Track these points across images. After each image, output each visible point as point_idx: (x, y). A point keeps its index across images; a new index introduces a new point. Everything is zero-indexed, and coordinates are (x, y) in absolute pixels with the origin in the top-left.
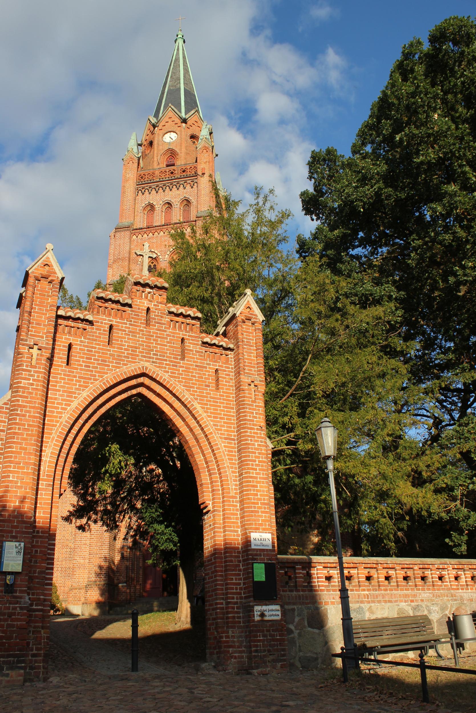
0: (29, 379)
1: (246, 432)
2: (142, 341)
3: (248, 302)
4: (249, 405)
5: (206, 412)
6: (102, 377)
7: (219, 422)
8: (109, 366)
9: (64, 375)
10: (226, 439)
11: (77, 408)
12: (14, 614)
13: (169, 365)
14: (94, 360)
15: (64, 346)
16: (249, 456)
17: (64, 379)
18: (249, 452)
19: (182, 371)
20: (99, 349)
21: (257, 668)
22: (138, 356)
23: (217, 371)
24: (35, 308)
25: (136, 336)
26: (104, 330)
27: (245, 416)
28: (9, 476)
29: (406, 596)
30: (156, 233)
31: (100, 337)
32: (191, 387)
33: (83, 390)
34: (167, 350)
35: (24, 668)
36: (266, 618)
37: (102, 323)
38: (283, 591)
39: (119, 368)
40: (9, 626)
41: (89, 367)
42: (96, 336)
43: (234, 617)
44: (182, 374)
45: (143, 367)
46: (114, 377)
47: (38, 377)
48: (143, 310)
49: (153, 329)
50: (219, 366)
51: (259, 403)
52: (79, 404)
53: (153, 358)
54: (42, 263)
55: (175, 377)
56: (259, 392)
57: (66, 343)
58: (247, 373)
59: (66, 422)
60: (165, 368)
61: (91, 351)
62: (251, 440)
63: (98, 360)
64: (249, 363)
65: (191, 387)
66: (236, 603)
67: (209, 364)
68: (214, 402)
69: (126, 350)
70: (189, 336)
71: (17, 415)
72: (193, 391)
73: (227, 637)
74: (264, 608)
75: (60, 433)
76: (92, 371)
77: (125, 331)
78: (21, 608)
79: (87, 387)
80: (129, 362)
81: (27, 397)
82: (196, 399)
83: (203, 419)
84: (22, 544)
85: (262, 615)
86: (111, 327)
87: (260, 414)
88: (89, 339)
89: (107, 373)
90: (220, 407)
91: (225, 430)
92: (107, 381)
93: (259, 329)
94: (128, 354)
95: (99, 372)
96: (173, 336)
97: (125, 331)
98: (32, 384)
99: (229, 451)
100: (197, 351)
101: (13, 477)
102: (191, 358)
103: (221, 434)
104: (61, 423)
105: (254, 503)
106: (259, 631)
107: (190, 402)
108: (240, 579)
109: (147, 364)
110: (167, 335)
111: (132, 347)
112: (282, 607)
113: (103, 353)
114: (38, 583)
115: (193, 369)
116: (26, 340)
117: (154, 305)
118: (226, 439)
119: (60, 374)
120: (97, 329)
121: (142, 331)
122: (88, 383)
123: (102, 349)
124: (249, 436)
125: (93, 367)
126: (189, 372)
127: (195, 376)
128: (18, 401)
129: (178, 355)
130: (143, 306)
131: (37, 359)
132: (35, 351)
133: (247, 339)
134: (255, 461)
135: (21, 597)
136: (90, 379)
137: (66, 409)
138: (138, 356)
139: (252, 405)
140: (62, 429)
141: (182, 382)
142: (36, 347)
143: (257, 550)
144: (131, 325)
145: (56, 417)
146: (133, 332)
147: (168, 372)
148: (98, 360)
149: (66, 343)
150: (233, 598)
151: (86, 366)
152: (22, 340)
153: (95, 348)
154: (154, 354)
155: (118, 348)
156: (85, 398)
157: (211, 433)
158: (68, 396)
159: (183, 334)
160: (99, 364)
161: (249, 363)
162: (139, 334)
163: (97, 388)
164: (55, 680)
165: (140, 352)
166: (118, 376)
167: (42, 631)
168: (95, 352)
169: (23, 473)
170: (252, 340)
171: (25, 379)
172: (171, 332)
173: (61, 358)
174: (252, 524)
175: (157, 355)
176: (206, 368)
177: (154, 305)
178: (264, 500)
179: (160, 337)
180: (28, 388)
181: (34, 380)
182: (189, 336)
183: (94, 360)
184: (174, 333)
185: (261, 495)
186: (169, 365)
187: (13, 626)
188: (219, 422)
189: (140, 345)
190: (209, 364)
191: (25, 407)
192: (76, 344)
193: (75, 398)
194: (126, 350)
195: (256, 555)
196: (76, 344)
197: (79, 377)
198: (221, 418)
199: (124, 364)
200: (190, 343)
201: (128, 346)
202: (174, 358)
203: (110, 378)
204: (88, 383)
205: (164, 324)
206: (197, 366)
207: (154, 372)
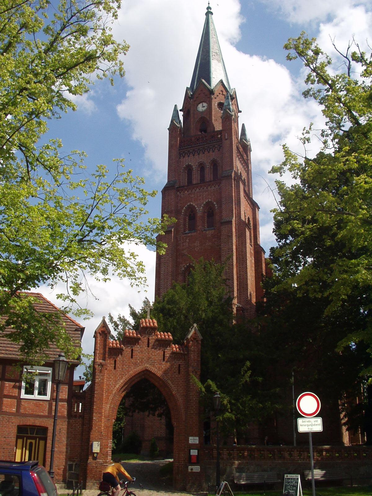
23: (179, 365)
74: (193, 467)
85: (192, 469)
171: (98, 379)
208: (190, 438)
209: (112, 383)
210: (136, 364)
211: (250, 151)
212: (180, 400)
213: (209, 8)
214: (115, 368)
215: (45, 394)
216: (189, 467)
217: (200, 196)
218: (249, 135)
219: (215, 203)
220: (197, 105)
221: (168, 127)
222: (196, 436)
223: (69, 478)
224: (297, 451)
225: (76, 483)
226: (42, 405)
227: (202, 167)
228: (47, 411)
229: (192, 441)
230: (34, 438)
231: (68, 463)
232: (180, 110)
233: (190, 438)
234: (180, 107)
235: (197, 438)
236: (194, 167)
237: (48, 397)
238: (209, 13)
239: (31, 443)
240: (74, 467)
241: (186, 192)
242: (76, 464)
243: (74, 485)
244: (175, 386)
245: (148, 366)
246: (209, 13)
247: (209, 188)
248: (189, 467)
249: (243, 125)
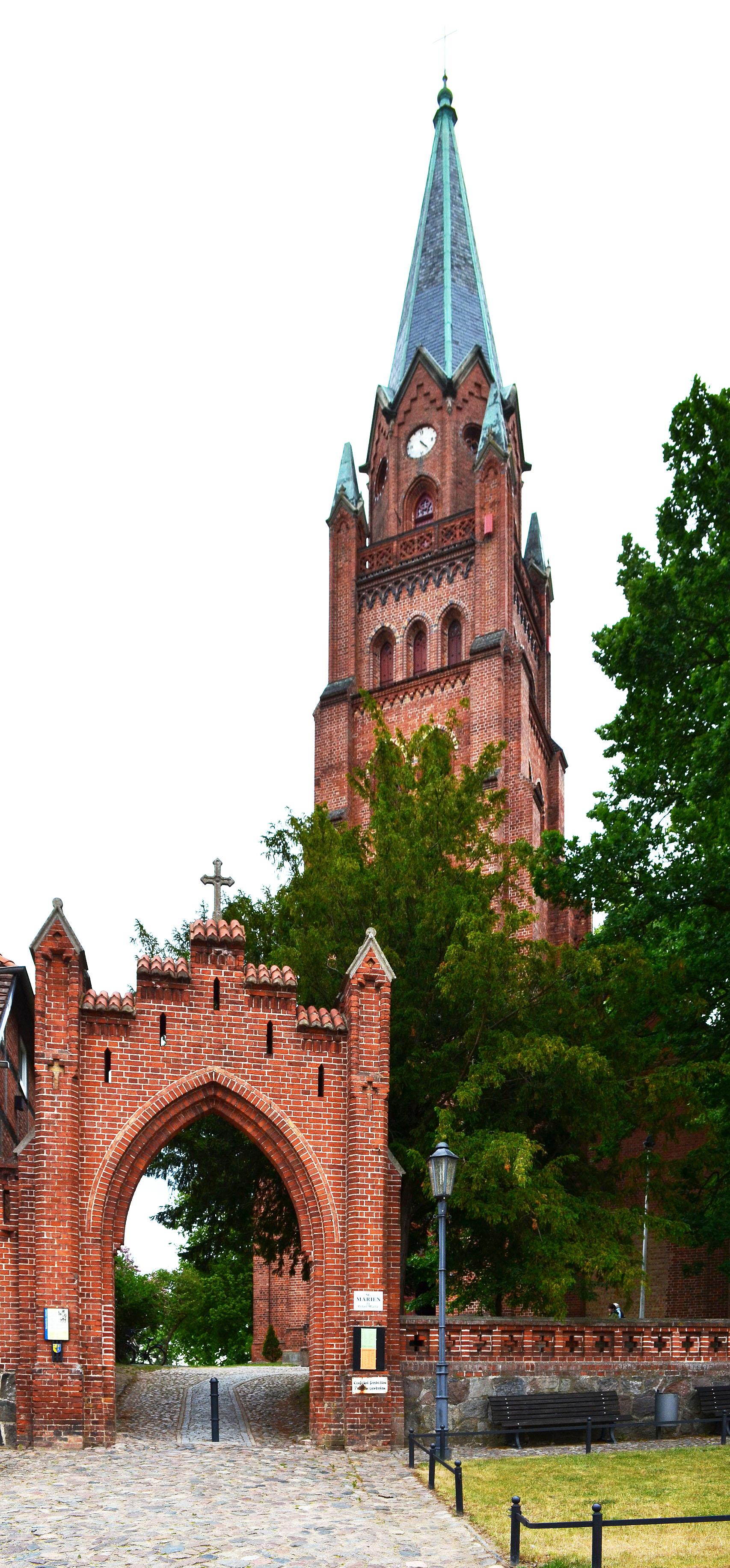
0: (53, 1110)
1: (356, 1158)
3: (371, 950)
4: (362, 1118)
5: (303, 1131)
6: (154, 1094)
7: (321, 1144)
9: (103, 1096)
11: (123, 1140)
12: (66, 1383)
13: (249, 1066)
14: (142, 1070)
15: (99, 1055)
16: (357, 1191)
17: (103, 1102)
18: (358, 1186)
19: (269, 1073)
20: (147, 1053)
21: (352, 1444)
22: (203, 1057)
24: (50, 1005)
25: (199, 1028)
26: (153, 1024)
27: (355, 1135)
28: (43, 1235)
29: (592, 1367)
32: (282, 1097)
33: (130, 1115)
34: (246, 1043)
36: (365, 1392)
37: (149, 1013)
38: (409, 1359)
39: (177, 1078)
40: (61, 1394)
41: (135, 1081)
42: (143, 1035)
43: (333, 1389)
44: (268, 1079)
45: (211, 1074)
47: (64, 1105)
50: (325, 1060)
51: (377, 1114)
52: (126, 1135)
53: (225, 1059)
57: (101, 1049)
58: (363, 1069)
59: (111, 1159)
60: (244, 1071)
61: (137, 1058)
62: (362, 1169)
63: (147, 1070)
64: (367, 1052)
65: (282, 1097)
66: (337, 1373)
67: (310, 1059)
68: (315, 1115)
69: (185, 1050)
70: (280, 1017)
72: (285, 1102)
73: (322, 1410)
75: (105, 1174)
76: (140, 1087)
77: (183, 1021)
78: (73, 1377)
79: (134, 1110)
80: (191, 1067)
81: (52, 1134)
82: (289, 1114)
84: (66, 1311)
85: (362, 1388)
88: (132, 1040)
89: (161, 1088)
91: (330, 1156)
93: (386, 996)
94: (189, 1056)
95: (149, 1088)
96: (255, 1021)
97: (183, 1021)
98: (57, 1116)
99: (335, 1184)
100: (291, 1041)
101: (48, 1235)
102: (282, 1052)
103: (324, 1161)
104: (105, 1161)
107: (279, 1118)
108: (343, 1346)
109: (217, 1069)
110: (246, 1020)
111: (194, 1045)
112: (389, 1379)
113: (153, 1059)
114: (93, 1350)
115: (286, 1069)
117: (226, 974)
119: (97, 1096)
120: (142, 1024)
121: (209, 1018)
122: (135, 1104)
123: (152, 1053)
124: (359, 1163)
125: (141, 1081)
126: (278, 1074)
127: (288, 1080)
128: (43, 1140)
129: (263, 1050)
130: (208, 978)
131: (60, 1081)
132: (56, 1070)
133: (366, 1013)
134: (366, 1197)
135: (71, 1366)
136: (138, 1098)
138: (203, 1057)
140: (107, 1170)
141: (268, 1090)
144: (191, 1010)
145: (98, 1154)
147: (247, 1077)
149: (101, 1049)
150: (333, 1367)
151: (131, 1081)
153: (142, 1052)
154: (226, 1053)
155: (174, 1049)
156: (133, 1126)
157: (310, 1160)
158: (110, 1125)
159: (269, 1016)
160: (148, 1076)
161: (367, 1052)
162: (204, 1023)
164: (119, 1446)
165: (206, 1052)
166: (176, 1090)
167: (103, 1399)
168: (143, 1058)
169: (60, 1230)
170: (375, 1014)
171: (48, 1110)
172: (252, 1015)
173: (96, 1073)
174: (356, 1280)
176: (304, 1065)
177: (226, 974)
178: (376, 1248)
179: (234, 1025)
180: (53, 1122)
182: (280, 1017)
183: (142, 1070)
184: (256, 1016)
185: (372, 1243)
186: (249, 1066)
187: (66, 1395)
188: (321, 1144)
189: (205, 1040)
190: (310, 1059)
191: (51, 1146)
192: (115, 1050)
194: (185, 1050)
195: (360, 1318)
196: (115, 1050)
197: (123, 1097)
198: (324, 1138)
199: (184, 1073)
200: (280, 1029)
201: (188, 1044)
202: (256, 1055)
203: (165, 1093)
205: (241, 1003)
206: (290, 1064)
207: (227, 1080)
208: (357, 1294)
209: (102, 1125)
210: (176, 1066)
211: (550, 598)
212: (324, 1178)
213: (445, 94)
216: (354, 1380)
217: (414, 716)
218: (549, 553)
220: (408, 440)
221: (328, 516)
222: (374, 1288)
227: (418, 629)
232: (363, 469)
233: (357, 1294)
234: (361, 459)
236: (397, 634)
238: (446, 113)
246: (446, 113)
247: (438, 691)
248: (354, 1380)
249: (534, 518)
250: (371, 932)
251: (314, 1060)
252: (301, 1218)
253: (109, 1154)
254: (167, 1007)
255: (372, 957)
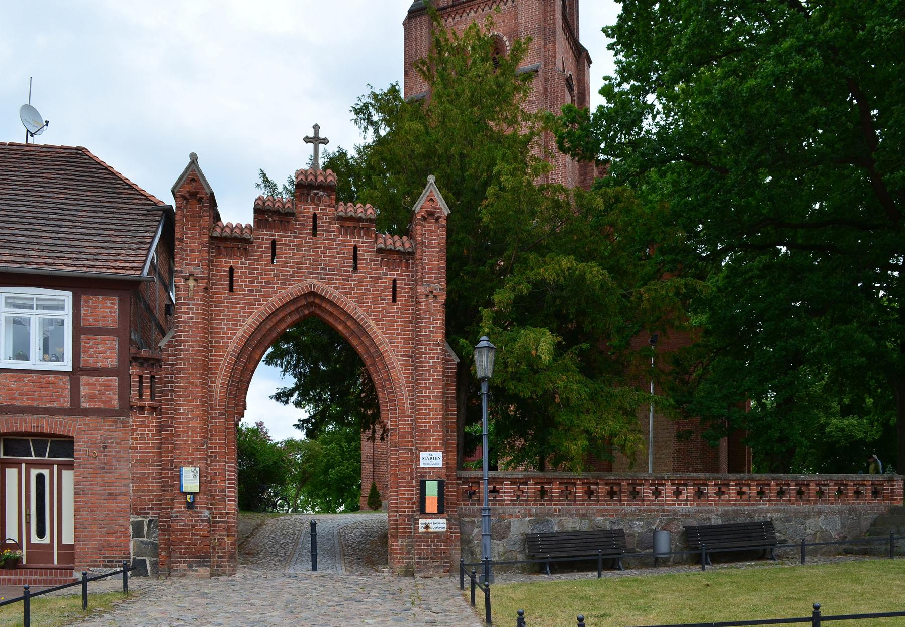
1: (421, 349)
2: (309, 255)
5: (380, 329)
8: (273, 288)
9: (228, 302)
10: (402, 356)
11: (243, 336)
13: (339, 280)
15: (224, 271)
17: (228, 307)
18: (422, 370)
20: (262, 269)
22: (304, 273)
23: (394, 281)
26: (266, 248)
30: (465, 14)
31: (262, 256)
34: (337, 262)
35: (209, 566)
36: (430, 530)
37: (263, 239)
39: (284, 288)
41: (252, 291)
42: (258, 256)
43: (405, 529)
44: (354, 289)
46: (280, 300)
48: (308, 217)
49: (320, 239)
50: (398, 275)
52: (245, 332)
54: (187, 179)
55: (347, 293)
56: (438, 302)
59: (233, 351)
60: (335, 283)
61: (254, 273)
62: (426, 358)
66: (408, 516)
67: (386, 274)
71: (181, 350)
73: (397, 545)
74: (429, 521)
78: (202, 521)
79: (251, 313)
81: (188, 332)
82: (370, 315)
83: (377, 336)
84: (197, 469)
85: (427, 527)
86: (274, 243)
87: (438, 328)
88: (250, 260)
90: (397, 321)
92: (273, 305)
93: (443, 226)
95: (263, 296)
96: (344, 245)
98: (192, 318)
102: (365, 268)
105: (425, 423)
106: (423, 541)
107: (363, 319)
109: (315, 281)
110: (338, 245)
112: (448, 520)
116: (181, 272)
117: (322, 209)
118: (402, 356)
121: (308, 243)
122: (252, 309)
123: (265, 270)
124: (423, 353)
125: (257, 291)
126: (362, 285)
127: (369, 290)
128: (180, 336)
129: (350, 267)
131: (194, 291)
132: (191, 283)
133: (428, 239)
134: (429, 379)
135: (201, 512)
136: (254, 304)
137: (232, 338)
139: (429, 319)
142: (191, 278)
143: (426, 468)
145: (223, 347)
146: (298, 246)
147: (338, 288)
148: (262, 282)
151: (249, 291)
152: (177, 271)
153: (257, 269)
154: (322, 269)
156: (250, 325)
157: (386, 351)
158: (233, 325)
160: (262, 287)
163: (263, 313)
166: (284, 297)
168: (258, 274)
171: (184, 313)
173: (222, 285)
175: (325, 269)
176: (382, 278)
177: (322, 209)
179: (328, 248)
180: (188, 323)
181: (193, 313)
186: (339, 280)
187: (197, 535)
189: (307, 260)
190: (386, 274)
191: (187, 341)
192: (237, 268)
193: (240, 325)
195: (425, 473)
200: (363, 251)
204: (252, 309)
205: (333, 231)
206: (371, 277)
208: (423, 454)
209: (226, 325)
212: (397, 365)
214: (231, 289)
215: (59, 358)
216: (421, 521)
219: (505, 38)
222: (436, 449)
223: (135, 554)
224: (673, 484)
225: (155, 564)
226: (53, 383)
228: (68, 399)
229: (428, 461)
230: (49, 465)
231: (132, 519)
233: (423, 454)
235: (440, 454)
237: (66, 365)
239: (40, 478)
240: (146, 528)
241: (450, 19)
242: (150, 521)
243: (149, 568)
244: (384, 333)
245: (317, 284)
248: (421, 521)
250: (431, 179)
251: (389, 275)
252: (380, 395)
253: (232, 347)
254: (277, 235)
255: (432, 197)
